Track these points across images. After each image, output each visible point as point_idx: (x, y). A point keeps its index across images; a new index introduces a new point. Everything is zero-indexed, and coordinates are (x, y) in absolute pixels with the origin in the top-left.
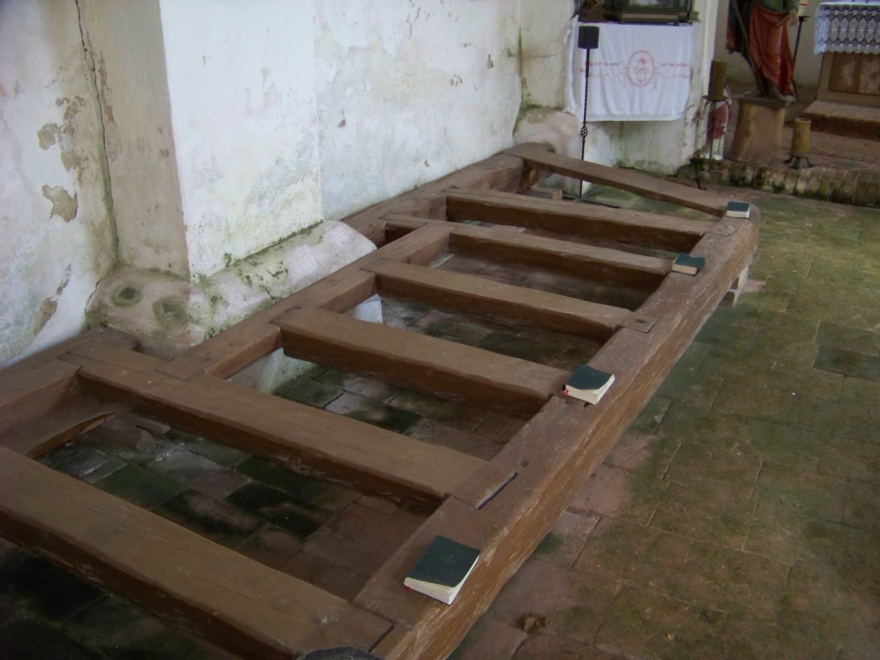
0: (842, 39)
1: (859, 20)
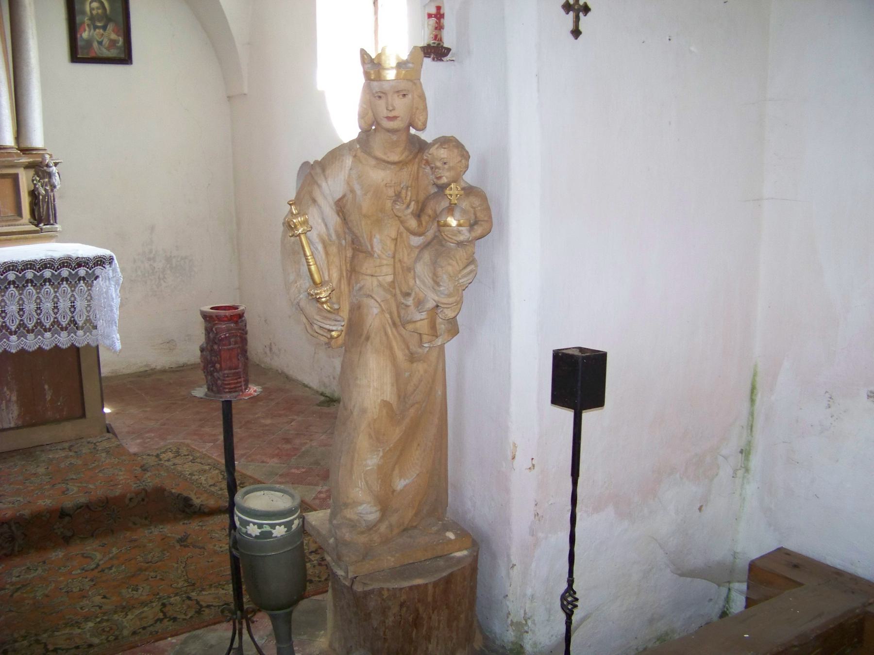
0: (64, 323)
1: (21, 288)
